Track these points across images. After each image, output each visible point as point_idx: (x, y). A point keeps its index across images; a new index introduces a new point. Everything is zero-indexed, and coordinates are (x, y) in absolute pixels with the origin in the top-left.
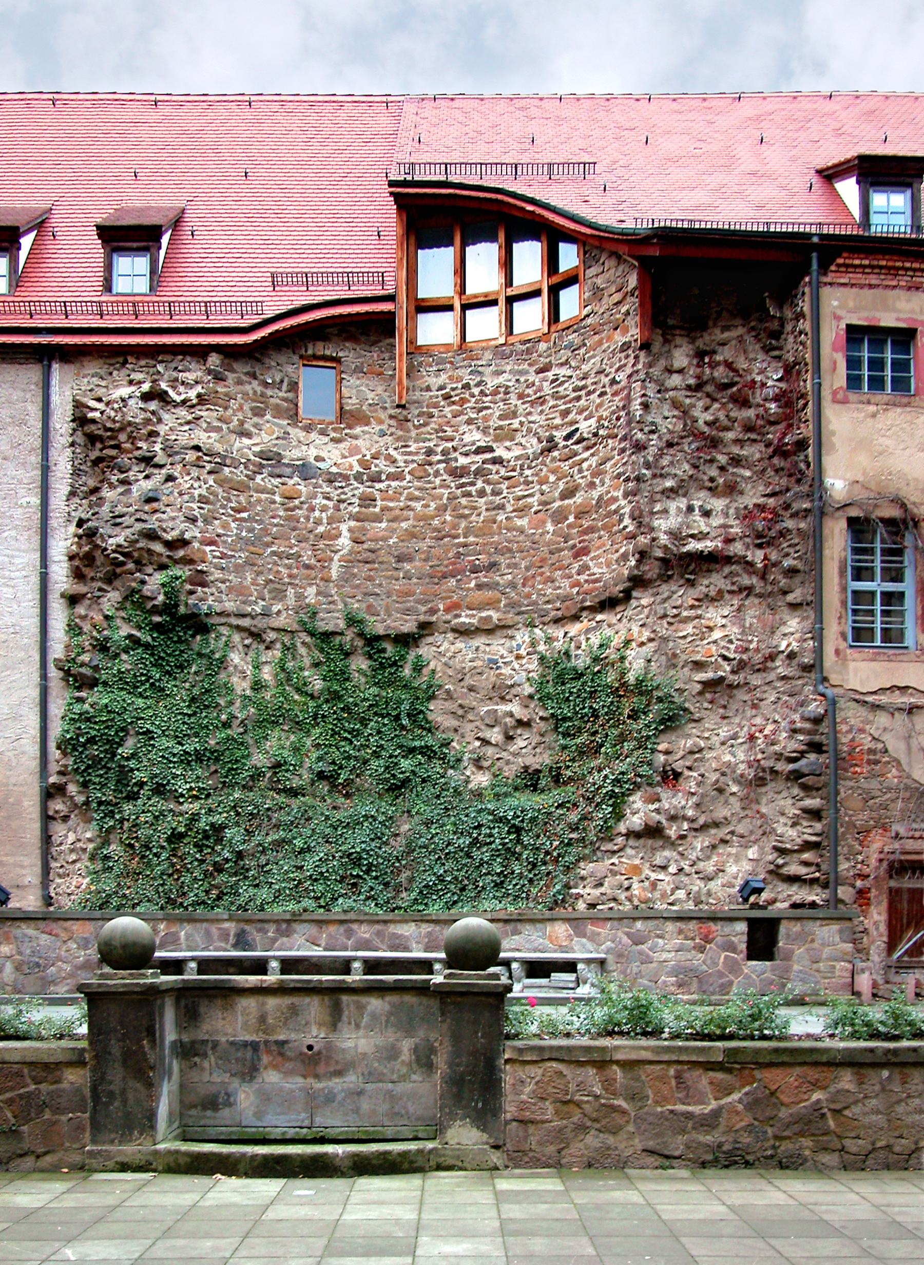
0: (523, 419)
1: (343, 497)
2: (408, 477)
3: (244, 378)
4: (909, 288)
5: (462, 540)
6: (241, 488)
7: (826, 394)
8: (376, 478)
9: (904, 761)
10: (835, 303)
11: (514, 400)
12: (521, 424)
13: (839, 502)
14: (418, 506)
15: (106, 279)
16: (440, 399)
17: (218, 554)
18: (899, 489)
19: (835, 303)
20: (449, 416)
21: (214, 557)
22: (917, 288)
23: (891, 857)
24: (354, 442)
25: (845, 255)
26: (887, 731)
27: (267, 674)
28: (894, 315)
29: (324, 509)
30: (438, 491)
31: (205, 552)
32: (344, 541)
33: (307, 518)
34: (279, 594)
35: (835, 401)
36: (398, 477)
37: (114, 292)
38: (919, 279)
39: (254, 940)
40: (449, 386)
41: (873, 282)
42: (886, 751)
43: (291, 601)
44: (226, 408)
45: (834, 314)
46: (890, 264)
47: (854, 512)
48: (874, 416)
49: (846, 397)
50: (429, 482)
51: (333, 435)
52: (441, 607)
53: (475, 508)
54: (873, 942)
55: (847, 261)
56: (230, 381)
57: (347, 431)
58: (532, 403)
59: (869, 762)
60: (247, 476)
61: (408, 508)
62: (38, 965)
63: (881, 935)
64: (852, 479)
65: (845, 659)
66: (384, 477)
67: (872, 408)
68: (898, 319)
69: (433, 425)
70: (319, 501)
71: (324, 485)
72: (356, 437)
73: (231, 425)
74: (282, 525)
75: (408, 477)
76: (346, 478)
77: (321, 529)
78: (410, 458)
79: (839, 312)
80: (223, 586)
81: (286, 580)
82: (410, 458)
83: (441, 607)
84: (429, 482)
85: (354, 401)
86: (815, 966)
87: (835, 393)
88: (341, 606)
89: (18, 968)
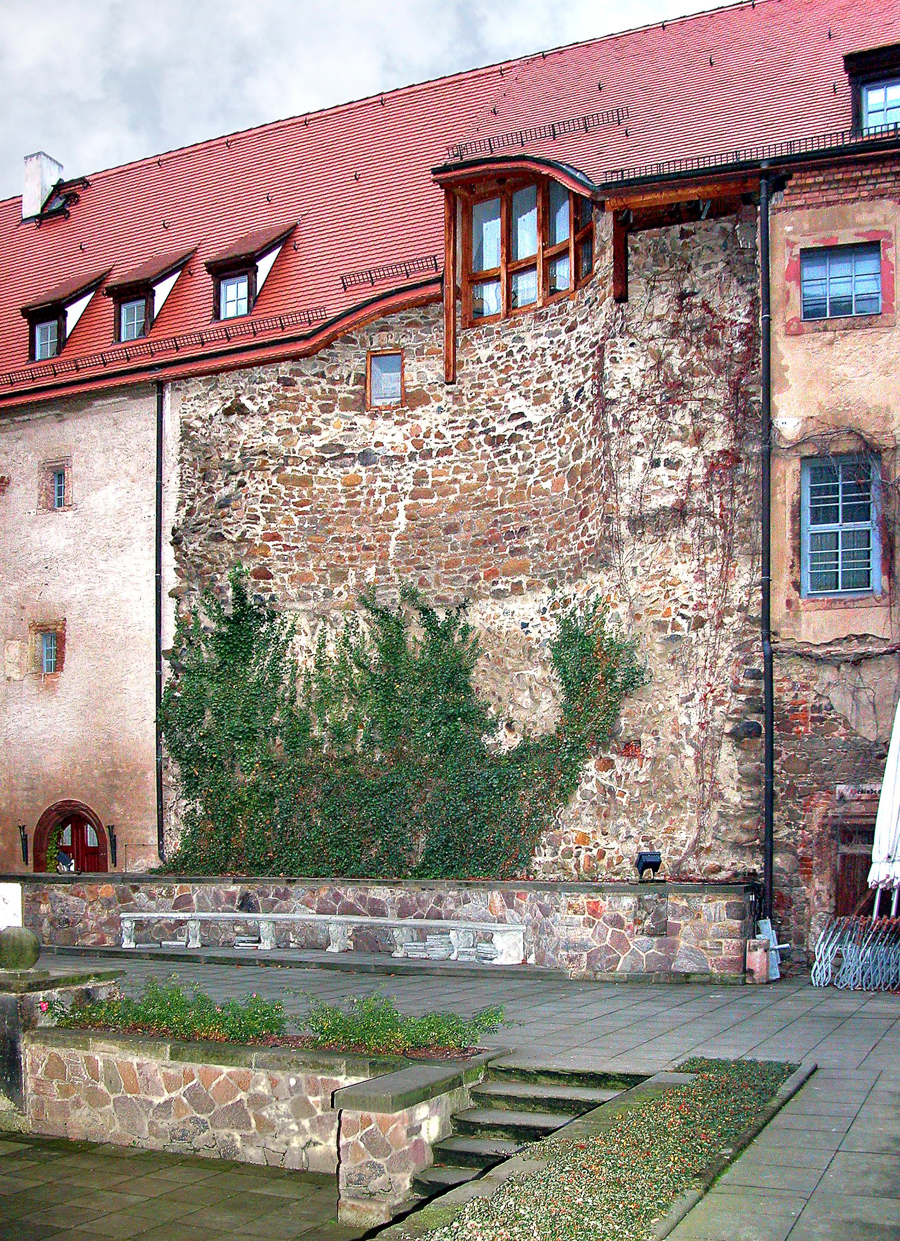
0: (556, 380)
1: (399, 478)
2: (455, 451)
3: (314, 379)
4: (872, 198)
5: (499, 508)
6: (305, 482)
7: (777, 327)
8: (428, 455)
9: (852, 717)
10: (789, 229)
11: (549, 361)
12: (555, 385)
13: (791, 442)
14: (462, 477)
15: (214, 308)
16: (489, 369)
17: (280, 547)
18: (858, 420)
19: (789, 229)
20: (497, 385)
21: (277, 550)
22: (882, 196)
23: (835, 821)
24: (416, 422)
25: (796, 175)
26: (831, 689)
27: (331, 650)
28: (855, 230)
29: (383, 490)
30: (479, 462)
31: (268, 548)
32: (401, 521)
33: (367, 502)
34: (341, 577)
35: (789, 334)
36: (446, 451)
37: (222, 318)
38: (882, 186)
39: (257, 902)
40: (496, 356)
41: (832, 198)
42: (832, 708)
43: (352, 581)
44: (295, 411)
45: (788, 241)
46: (847, 176)
47: (808, 451)
48: (831, 343)
49: (800, 327)
50: (473, 454)
51: (396, 418)
52: (482, 575)
53: (510, 474)
54: (814, 913)
55: (799, 182)
56: (299, 386)
57: (410, 413)
58: (563, 362)
59: (813, 719)
60: (309, 471)
61: (455, 481)
62: (67, 921)
63: (824, 905)
64: (806, 415)
65: (797, 610)
66: (434, 453)
67: (829, 335)
68: (857, 235)
69: (483, 396)
70: (379, 483)
71: (383, 468)
72: (418, 417)
73: (300, 426)
74: (344, 512)
75: (455, 451)
76: (401, 459)
77: (380, 510)
78: (456, 432)
79: (792, 238)
80: (286, 576)
81: (347, 563)
82: (456, 432)
83: (482, 575)
84: (473, 454)
85: (416, 383)
86: (701, 943)
87: (788, 325)
88: (397, 582)
89: (51, 923)
